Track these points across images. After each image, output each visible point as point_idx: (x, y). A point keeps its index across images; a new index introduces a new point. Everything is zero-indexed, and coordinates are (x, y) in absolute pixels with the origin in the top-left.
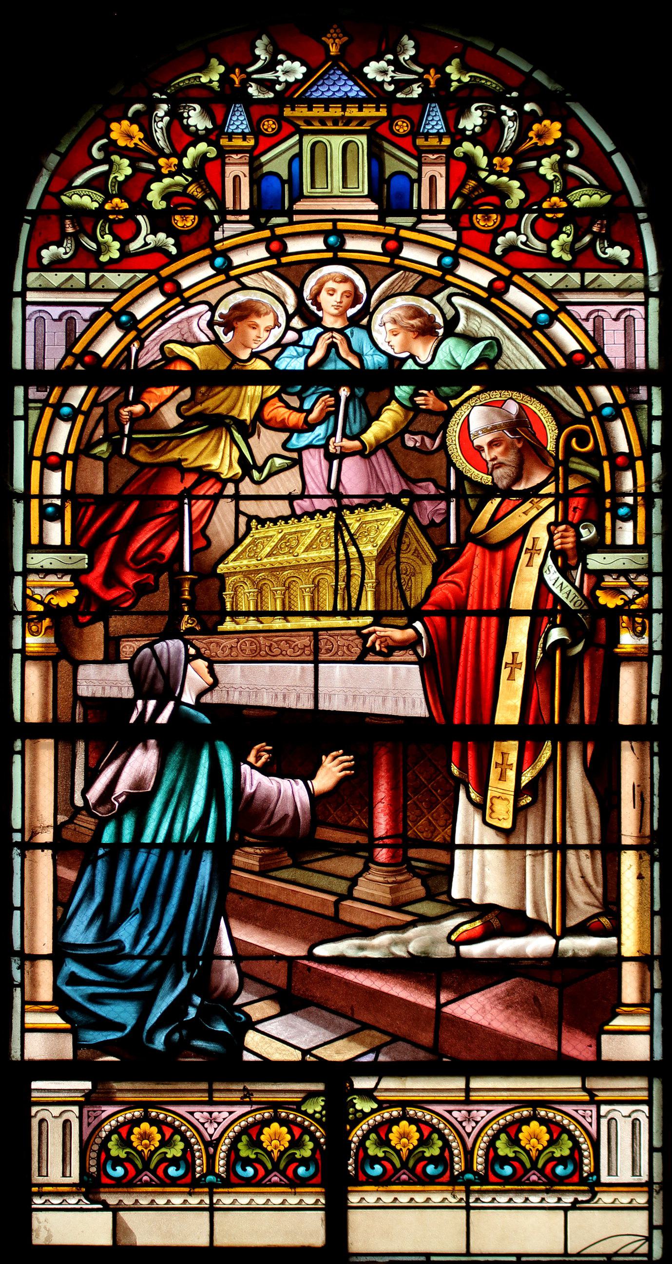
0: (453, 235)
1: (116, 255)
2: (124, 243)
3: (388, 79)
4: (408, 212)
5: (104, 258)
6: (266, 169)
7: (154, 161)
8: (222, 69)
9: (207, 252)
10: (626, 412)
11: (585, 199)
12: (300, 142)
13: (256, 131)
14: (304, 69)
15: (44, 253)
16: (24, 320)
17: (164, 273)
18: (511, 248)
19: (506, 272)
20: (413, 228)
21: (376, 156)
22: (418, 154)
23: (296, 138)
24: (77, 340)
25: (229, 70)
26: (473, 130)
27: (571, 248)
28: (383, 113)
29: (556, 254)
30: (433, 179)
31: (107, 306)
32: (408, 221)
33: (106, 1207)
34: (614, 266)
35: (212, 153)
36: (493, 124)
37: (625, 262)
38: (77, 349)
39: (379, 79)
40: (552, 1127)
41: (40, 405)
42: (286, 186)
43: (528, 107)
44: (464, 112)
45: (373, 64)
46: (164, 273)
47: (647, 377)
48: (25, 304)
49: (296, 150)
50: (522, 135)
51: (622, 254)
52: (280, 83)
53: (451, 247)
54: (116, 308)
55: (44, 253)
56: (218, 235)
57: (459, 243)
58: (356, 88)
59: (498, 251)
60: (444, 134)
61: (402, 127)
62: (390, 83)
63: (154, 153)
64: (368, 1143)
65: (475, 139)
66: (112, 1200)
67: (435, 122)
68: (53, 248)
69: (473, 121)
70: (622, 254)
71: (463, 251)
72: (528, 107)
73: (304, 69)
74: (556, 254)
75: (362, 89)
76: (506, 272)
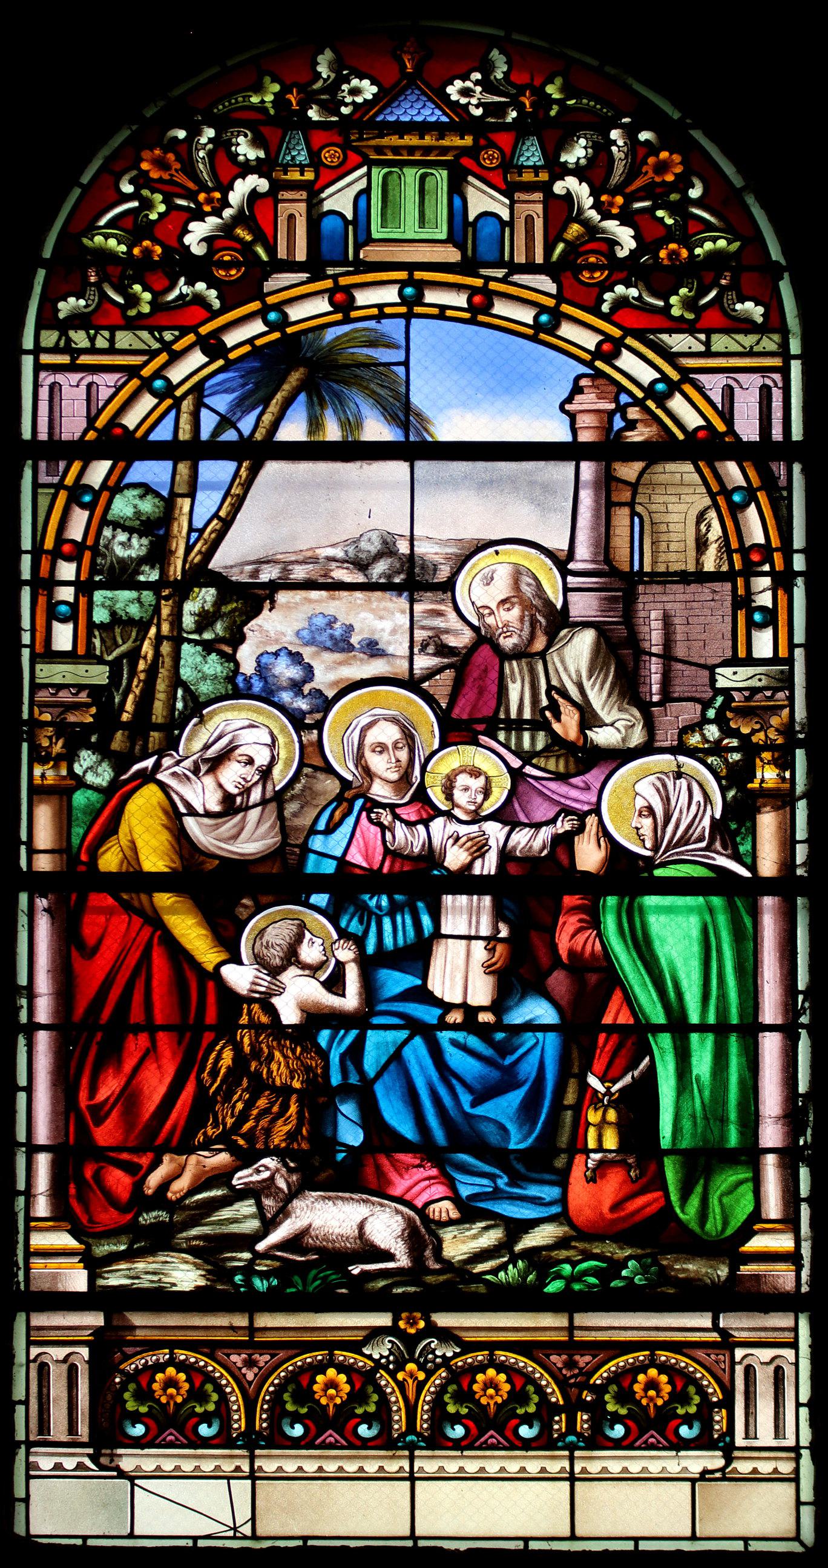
0: (552, 288)
1: (146, 309)
2: (156, 295)
3: (474, 101)
4: (499, 264)
5: (132, 313)
6: (327, 206)
7: (191, 196)
8: (276, 88)
9: (255, 306)
10: (761, 496)
11: (708, 246)
12: (369, 175)
13: (315, 162)
14: (375, 89)
15: (61, 305)
16: (36, 386)
17: (204, 330)
18: (621, 303)
19: (616, 332)
20: (504, 280)
21: (457, 188)
22: (509, 191)
23: (364, 169)
24: (100, 412)
25: (285, 90)
26: (577, 163)
27: (689, 304)
28: (468, 141)
29: (676, 312)
30: (529, 220)
31: (132, 372)
32: (500, 273)
33: (122, 1475)
34: (746, 326)
35: (263, 185)
36: (601, 149)
37: (760, 320)
38: (100, 423)
39: (463, 101)
40: (194, 1374)
41: (52, 491)
42: (351, 228)
43: (644, 136)
44: (566, 142)
45: (458, 84)
46: (204, 330)
47: (788, 451)
48: (38, 367)
49: (362, 184)
50: (633, 172)
51: (753, 310)
52: (346, 105)
53: (551, 302)
54: (146, 372)
55: (61, 305)
56: (269, 285)
57: (560, 298)
58: (438, 112)
59: (605, 308)
60: (541, 167)
61: (490, 159)
62: (477, 106)
63: (191, 185)
64: (447, 1398)
65: (579, 172)
66: (127, 1464)
67: (531, 154)
68: (72, 300)
69: (577, 153)
70: (753, 310)
71: (566, 308)
72: (644, 136)
73: (375, 89)
74: (676, 312)
75: (445, 113)
76: (616, 332)
